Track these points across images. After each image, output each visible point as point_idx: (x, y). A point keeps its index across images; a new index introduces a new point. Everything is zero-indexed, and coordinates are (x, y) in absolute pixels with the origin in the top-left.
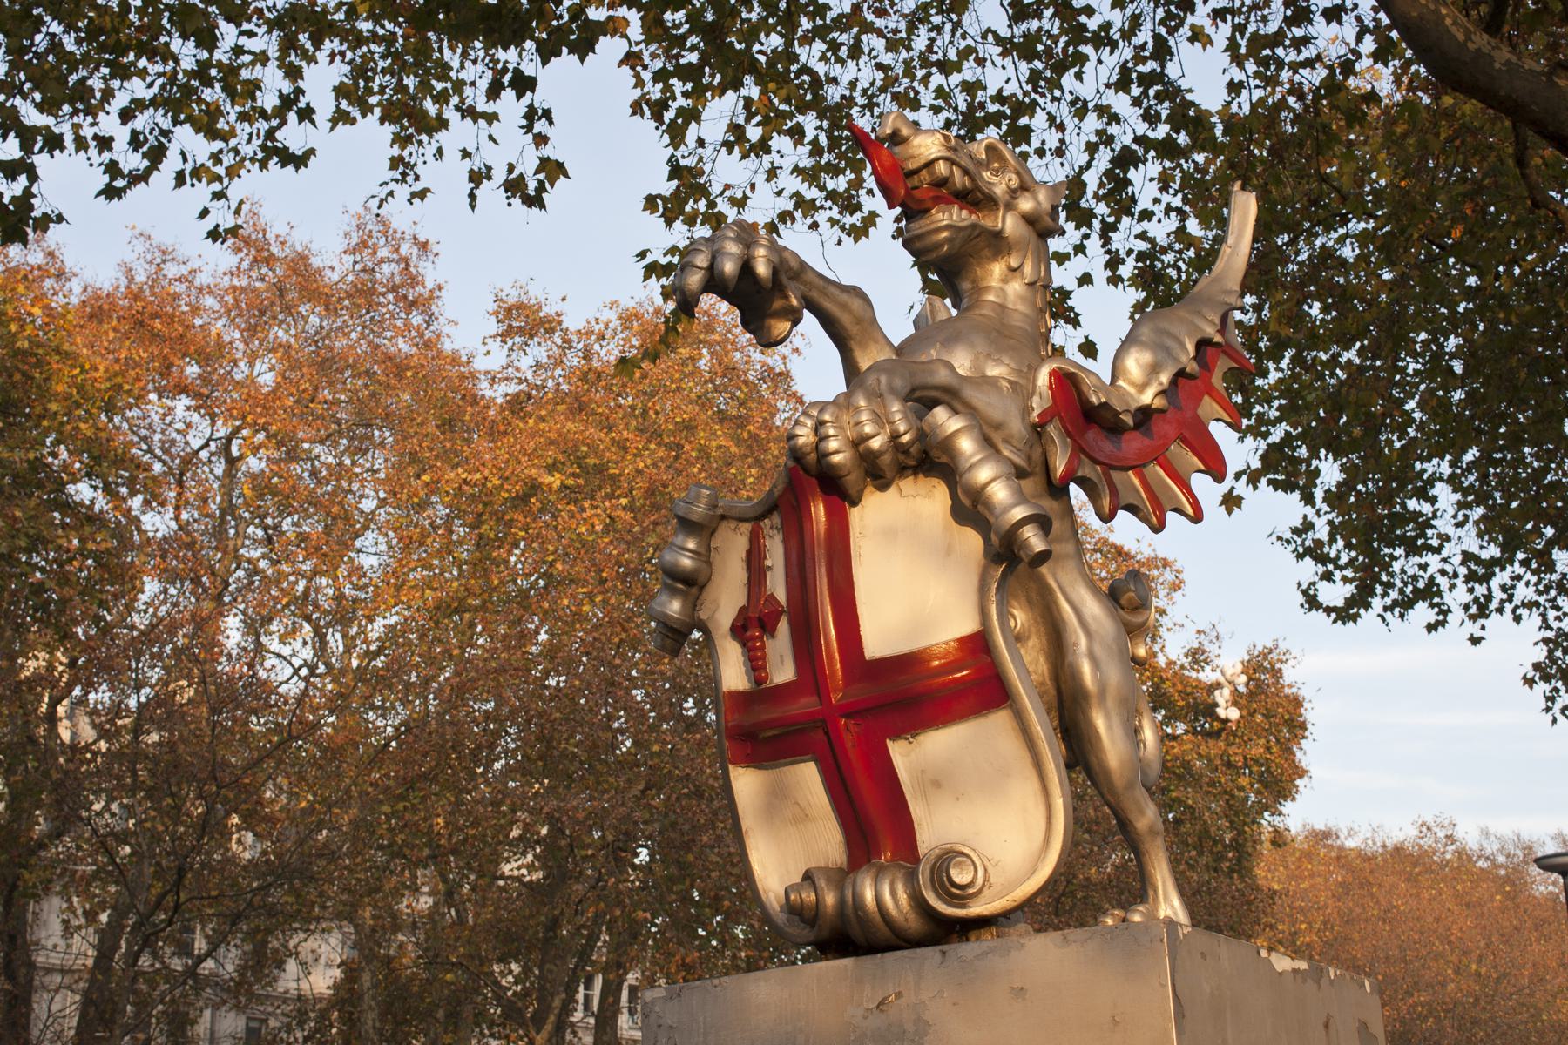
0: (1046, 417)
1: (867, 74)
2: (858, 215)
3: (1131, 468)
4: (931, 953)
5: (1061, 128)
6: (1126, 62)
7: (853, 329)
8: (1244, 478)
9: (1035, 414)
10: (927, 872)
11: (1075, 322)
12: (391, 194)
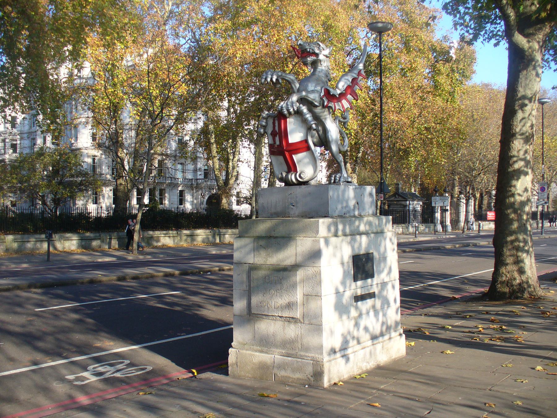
7: (291, 81)
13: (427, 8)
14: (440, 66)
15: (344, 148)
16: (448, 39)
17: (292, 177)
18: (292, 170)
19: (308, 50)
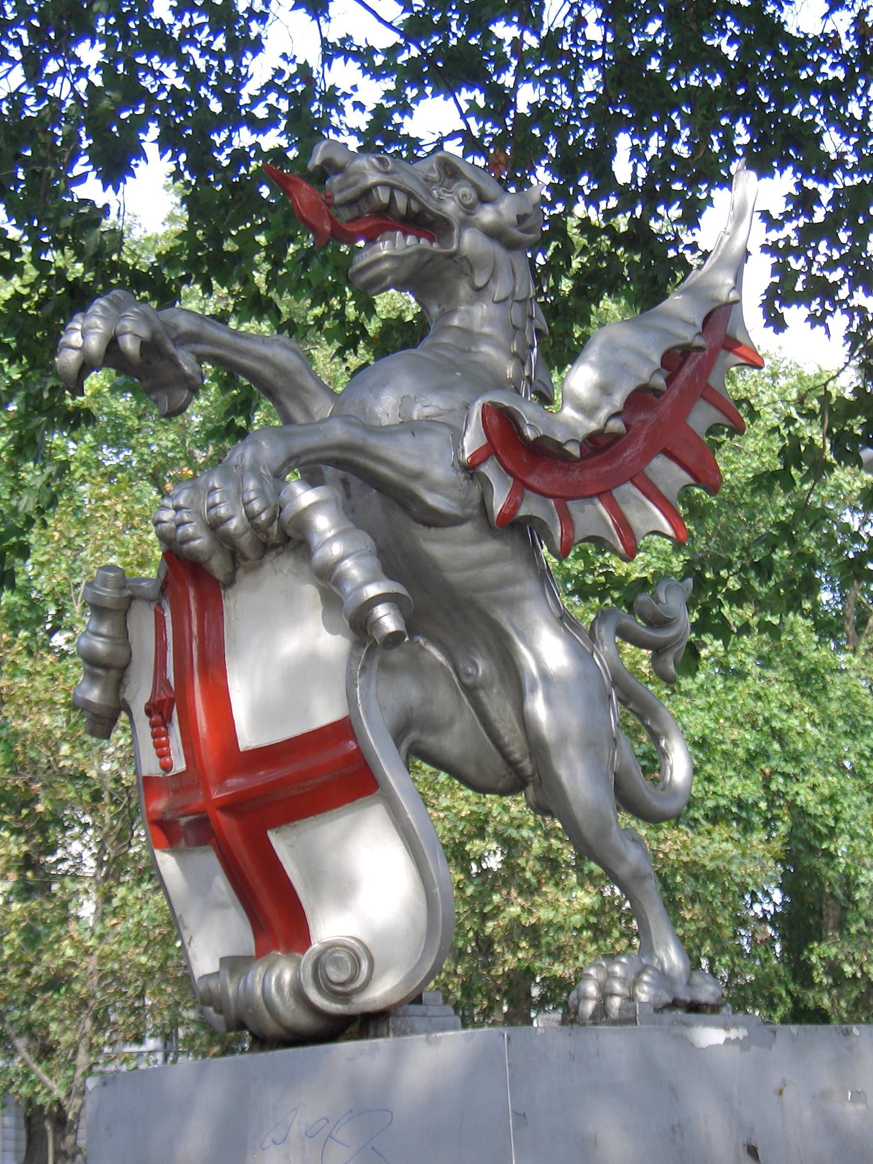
0: (480, 457)
7: (279, 382)
9: (467, 455)
10: (309, 968)
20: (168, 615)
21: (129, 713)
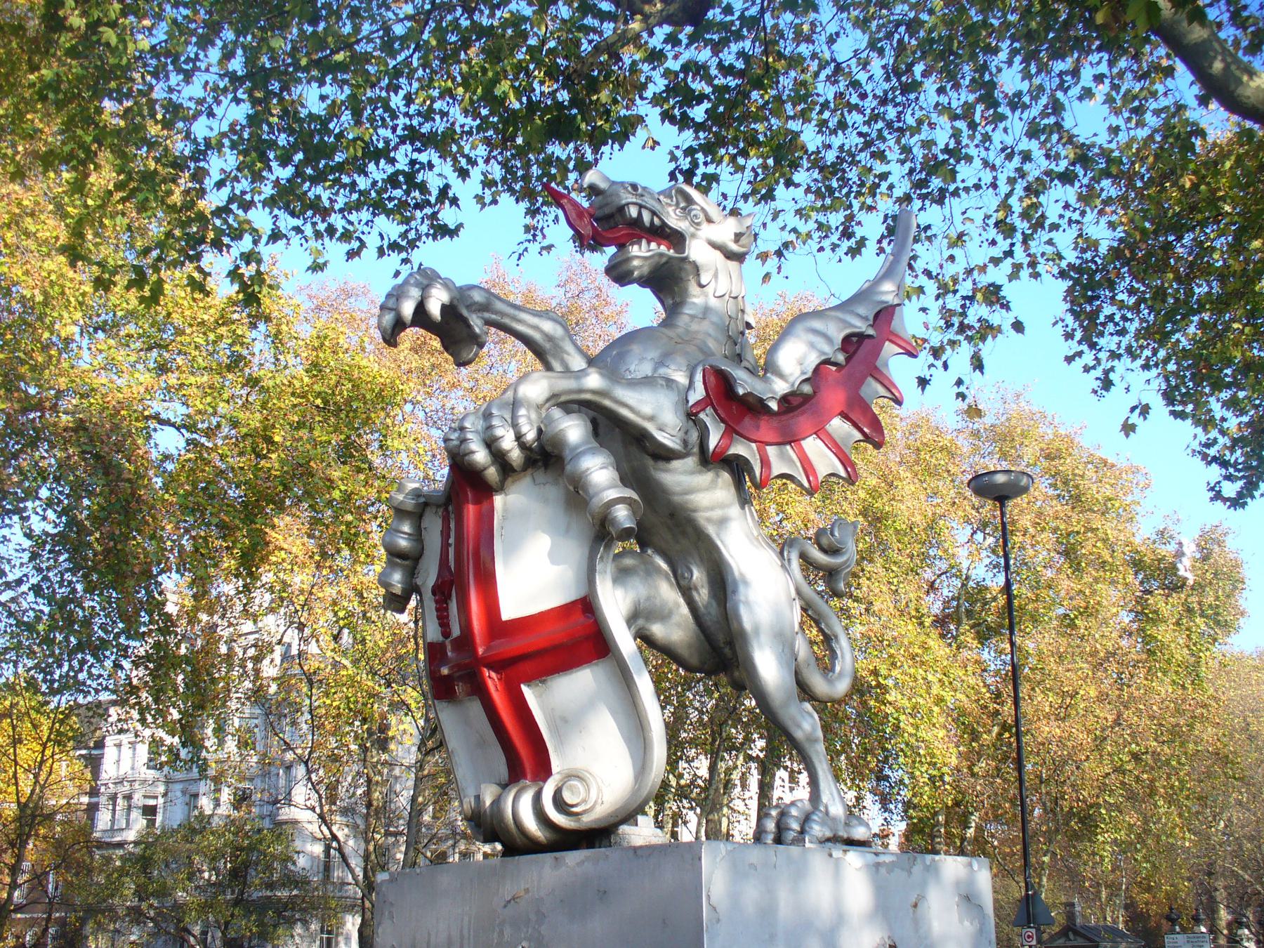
1: (854, 140)
2: (853, 240)
3: (755, 441)
4: (548, 857)
5: (993, 168)
6: (1035, 118)
7: (547, 346)
8: (1138, 411)
11: (1006, 306)
12: (526, 249)
13: (1113, 466)
14: (1157, 601)
15: (830, 682)
16: (1171, 537)
17: (522, 809)
18: (529, 776)
19: (633, 212)
20: (452, 525)
21: (419, 592)
